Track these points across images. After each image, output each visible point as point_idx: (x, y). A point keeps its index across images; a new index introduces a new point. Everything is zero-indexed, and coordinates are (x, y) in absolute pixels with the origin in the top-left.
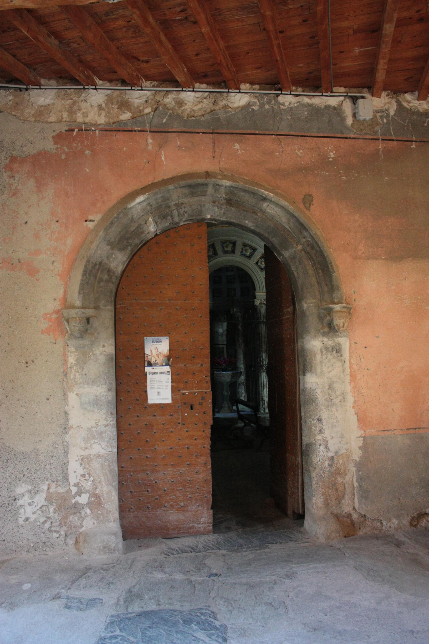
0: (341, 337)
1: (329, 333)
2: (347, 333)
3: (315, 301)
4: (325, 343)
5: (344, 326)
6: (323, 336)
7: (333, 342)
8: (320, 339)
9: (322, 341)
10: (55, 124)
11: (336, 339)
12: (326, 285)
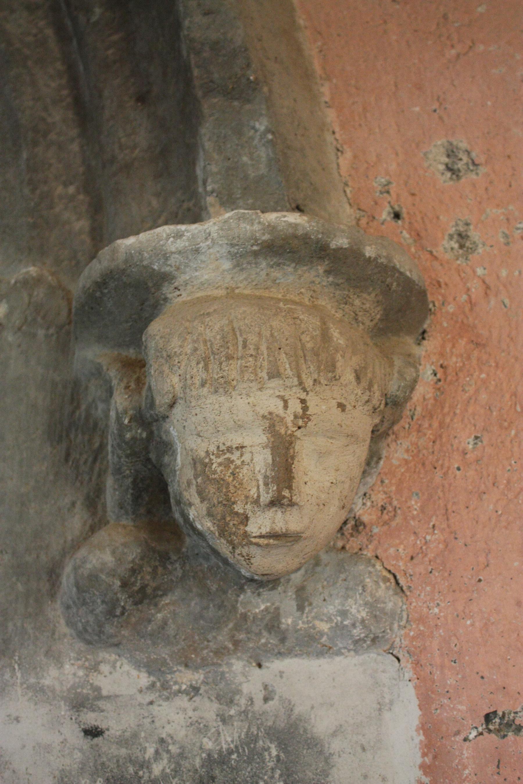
0: (310, 644)
1: (144, 597)
2: (383, 591)
3: (33, 270)
4: (115, 723)
5: (284, 472)
6: (94, 638)
7: (209, 709)
8: (51, 677)
9: (79, 703)
10: (385, 564)
11: (248, 679)
12: (142, 99)
